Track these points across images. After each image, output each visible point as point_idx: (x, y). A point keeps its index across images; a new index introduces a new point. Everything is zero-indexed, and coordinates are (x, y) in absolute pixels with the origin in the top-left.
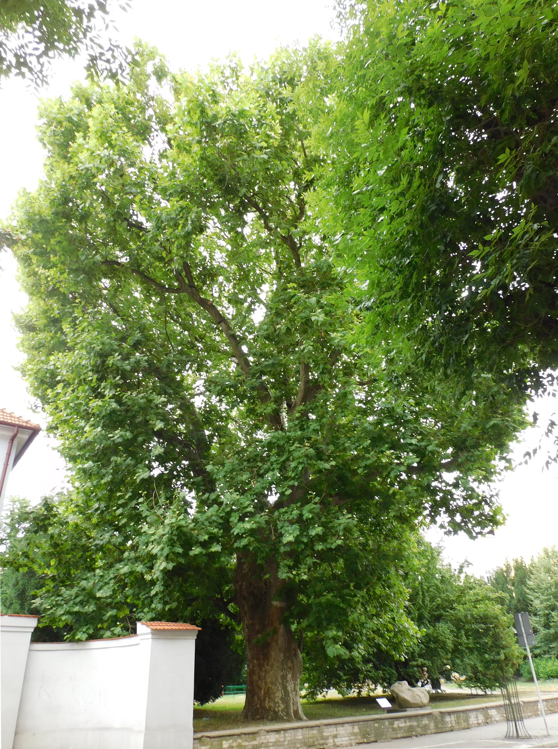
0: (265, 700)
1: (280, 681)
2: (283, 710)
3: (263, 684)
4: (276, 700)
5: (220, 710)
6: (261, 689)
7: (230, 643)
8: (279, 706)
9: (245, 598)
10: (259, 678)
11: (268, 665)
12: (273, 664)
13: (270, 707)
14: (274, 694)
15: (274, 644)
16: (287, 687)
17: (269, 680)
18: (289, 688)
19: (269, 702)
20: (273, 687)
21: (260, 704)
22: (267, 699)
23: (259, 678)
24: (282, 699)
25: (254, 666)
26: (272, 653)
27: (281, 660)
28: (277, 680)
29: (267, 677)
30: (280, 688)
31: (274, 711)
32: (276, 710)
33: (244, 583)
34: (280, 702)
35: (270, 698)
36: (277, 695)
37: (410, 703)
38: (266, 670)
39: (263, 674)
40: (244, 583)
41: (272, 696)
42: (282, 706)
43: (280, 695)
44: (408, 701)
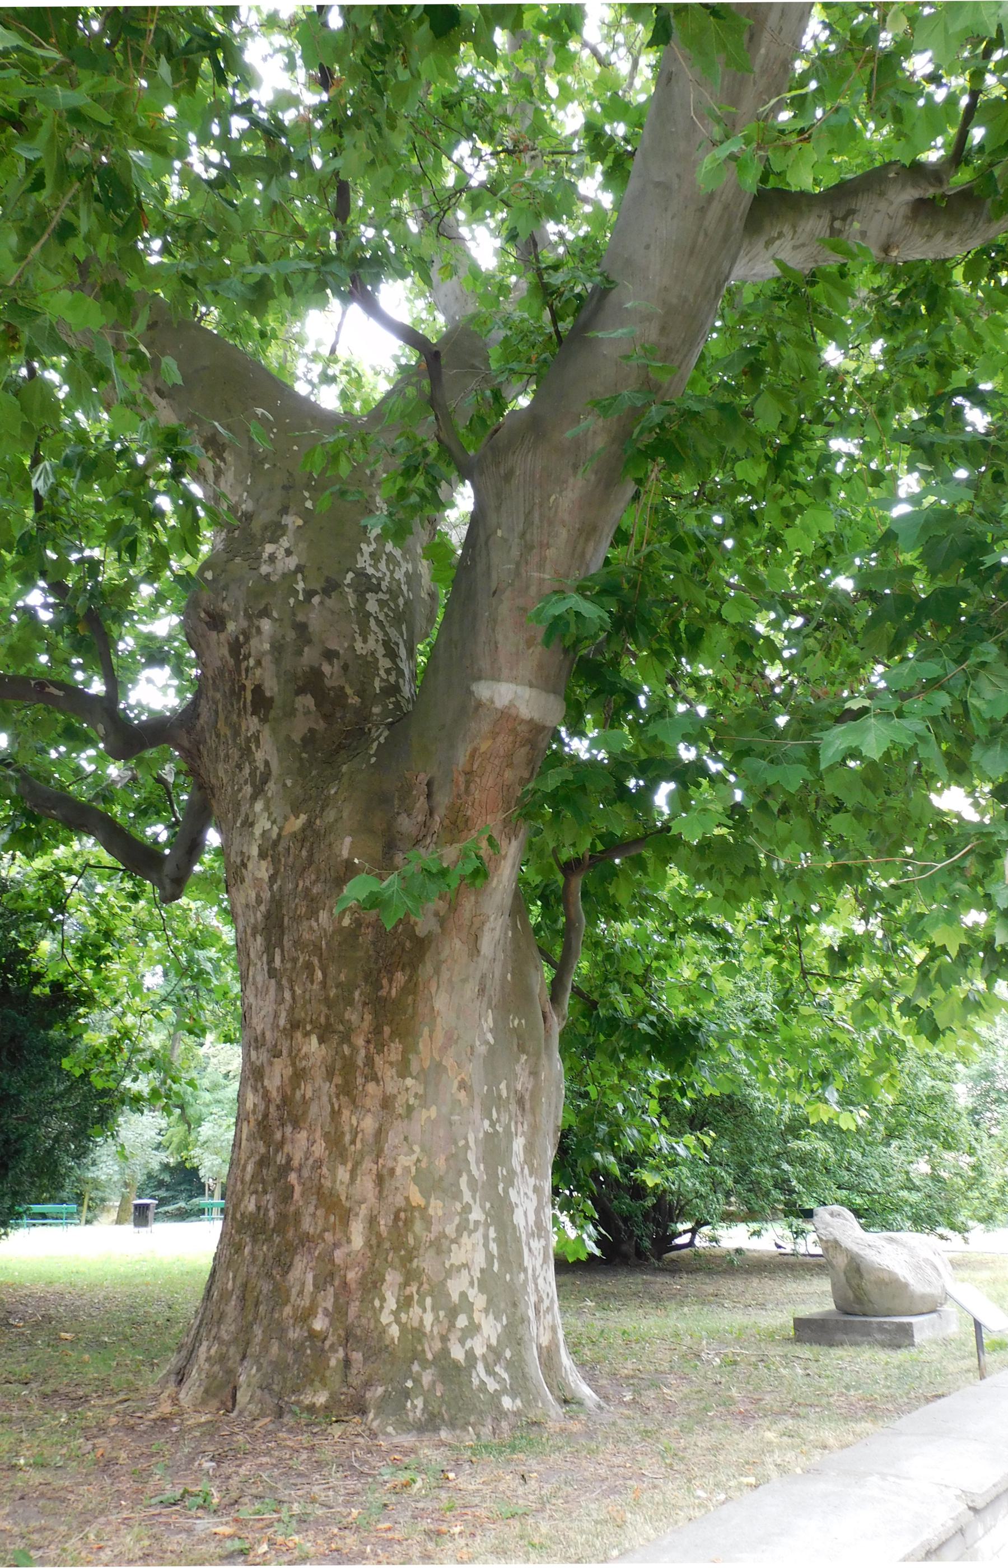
0: (372, 1284)
1: (478, 1171)
2: (495, 1352)
3: (366, 1185)
4: (456, 1287)
5: (39, 1289)
6: (346, 1217)
7: (65, 1049)
8: (474, 1329)
9: (261, 703)
10: (335, 1142)
11: (403, 1070)
12: (439, 1067)
13: (417, 1333)
14: (440, 1246)
15: (455, 946)
16: (511, 1208)
17: (405, 1161)
18: (518, 1218)
19: (405, 1303)
20: (436, 1207)
21: (338, 1313)
22: (392, 1278)
23: (335, 1142)
24: (486, 1282)
25: (299, 1076)
26: (441, 1002)
27: (482, 1049)
28: (458, 1163)
29: (393, 1139)
30: (476, 1215)
31: (443, 1361)
32: (458, 1353)
33: (266, 625)
34: (479, 1301)
35: (410, 1276)
36: (457, 1256)
37: (912, 1296)
38: (387, 1103)
39: (369, 1124)
40: (266, 625)
41: (426, 1263)
42: (491, 1329)
43: (479, 1260)
44: (906, 1286)
